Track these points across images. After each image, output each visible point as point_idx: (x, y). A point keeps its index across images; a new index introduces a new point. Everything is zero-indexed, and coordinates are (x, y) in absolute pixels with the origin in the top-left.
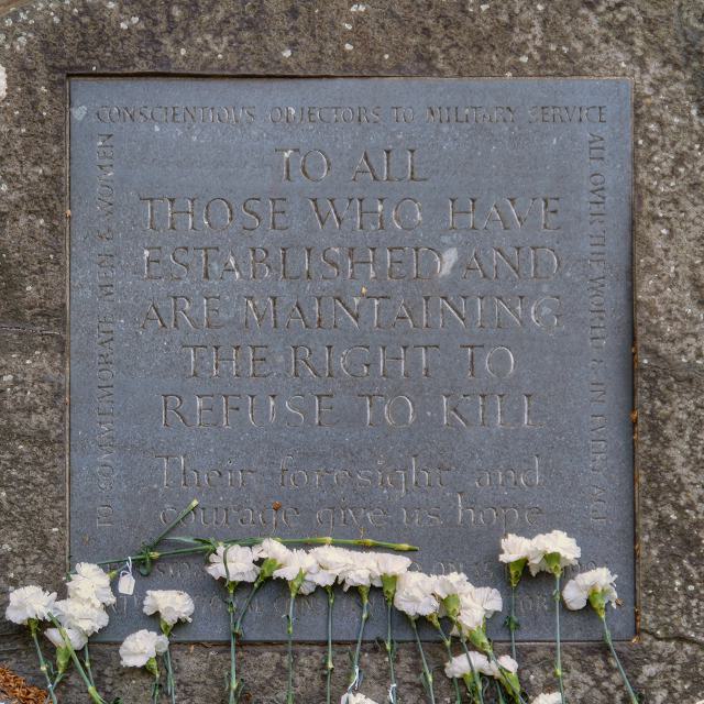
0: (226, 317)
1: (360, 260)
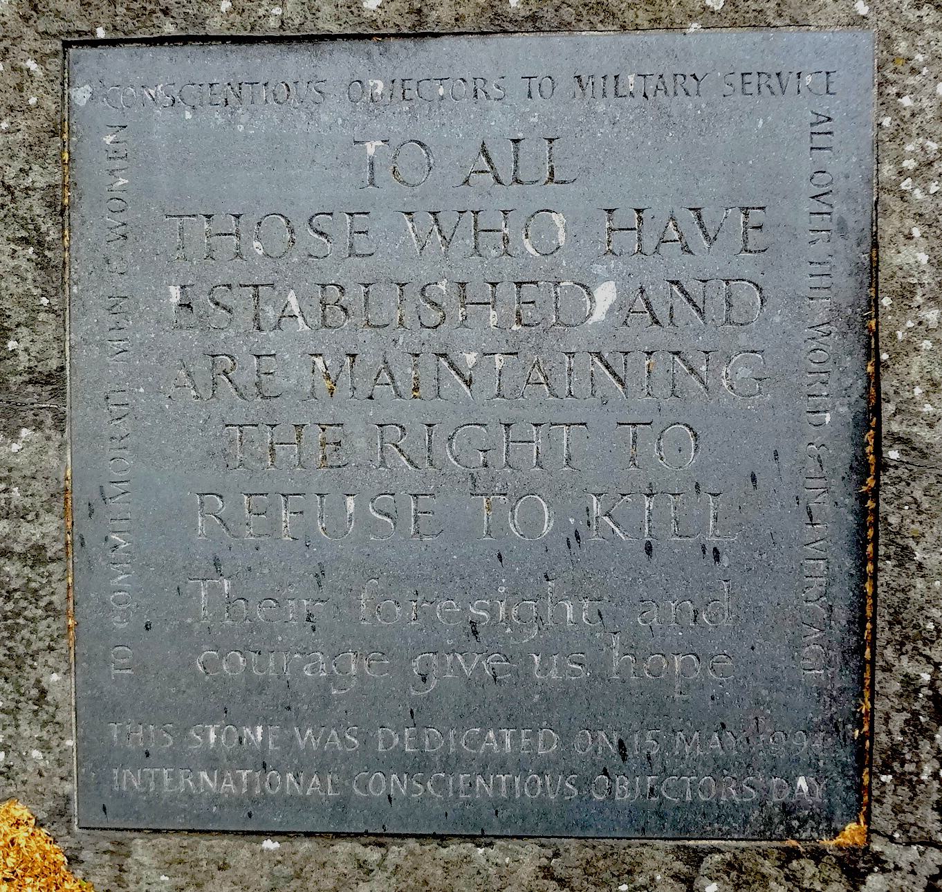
0: (285, 384)
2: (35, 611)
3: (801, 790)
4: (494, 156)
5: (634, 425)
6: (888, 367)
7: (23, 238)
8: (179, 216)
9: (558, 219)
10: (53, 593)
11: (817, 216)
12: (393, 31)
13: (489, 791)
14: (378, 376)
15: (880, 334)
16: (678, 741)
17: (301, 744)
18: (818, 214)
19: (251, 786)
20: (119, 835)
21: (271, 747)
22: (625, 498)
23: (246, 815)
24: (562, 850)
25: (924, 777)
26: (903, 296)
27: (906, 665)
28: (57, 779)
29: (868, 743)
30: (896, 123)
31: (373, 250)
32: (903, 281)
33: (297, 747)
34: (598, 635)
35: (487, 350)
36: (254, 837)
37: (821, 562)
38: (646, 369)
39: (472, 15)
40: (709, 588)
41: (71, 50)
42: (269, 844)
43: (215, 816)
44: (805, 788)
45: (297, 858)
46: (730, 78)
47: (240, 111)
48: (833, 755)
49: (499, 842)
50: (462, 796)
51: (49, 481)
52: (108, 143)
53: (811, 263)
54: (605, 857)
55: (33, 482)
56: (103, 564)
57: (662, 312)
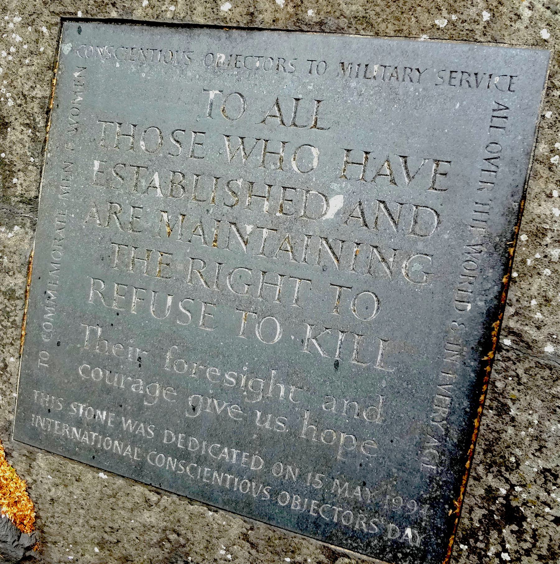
0: (146, 225)
1: (257, 194)
2: (7, 323)
3: (407, 536)
4: (282, 107)
5: (341, 287)
6: (516, 282)
7: (27, 124)
8: (105, 122)
9: (315, 151)
10: (16, 316)
11: (486, 172)
12: (235, 25)
13: (220, 481)
14: (195, 230)
15: (515, 259)
16: (335, 485)
17: (125, 426)
18: (487, 171)
19: (96, 442)
20: (31, 448)
21: (109, 424)
22: (327, 330)
23: (92, 457)
24: (255, 527)
25: (490, 554)
26: (536, 236)
27: (490, 480)
28: (7, 412)
29: (457, 520)
30: (555, 116)
31: (204, 155)
32: (538, 225)
33: (122, 428)
34: (297, 409)
35: (259, 225)
36: (95, 469)
37: (447, 398)
38: (354, 254)
39: (283, 18)
40: (370, 397)
41: (65, 23)
42: (101, 475)
43: (77, 452)
44: (410, 536)
45: (115, 486)
46: (442, 73)
47: (144, 65)
48: (433, 521)
49: (221, 512)
50: (204, 480)
51: (22, 256)
52: (76, 76)
53: (476, 203)
54: (280, 538)
55: (14, 255)
56: (42, 305)
57: (371, 220)
